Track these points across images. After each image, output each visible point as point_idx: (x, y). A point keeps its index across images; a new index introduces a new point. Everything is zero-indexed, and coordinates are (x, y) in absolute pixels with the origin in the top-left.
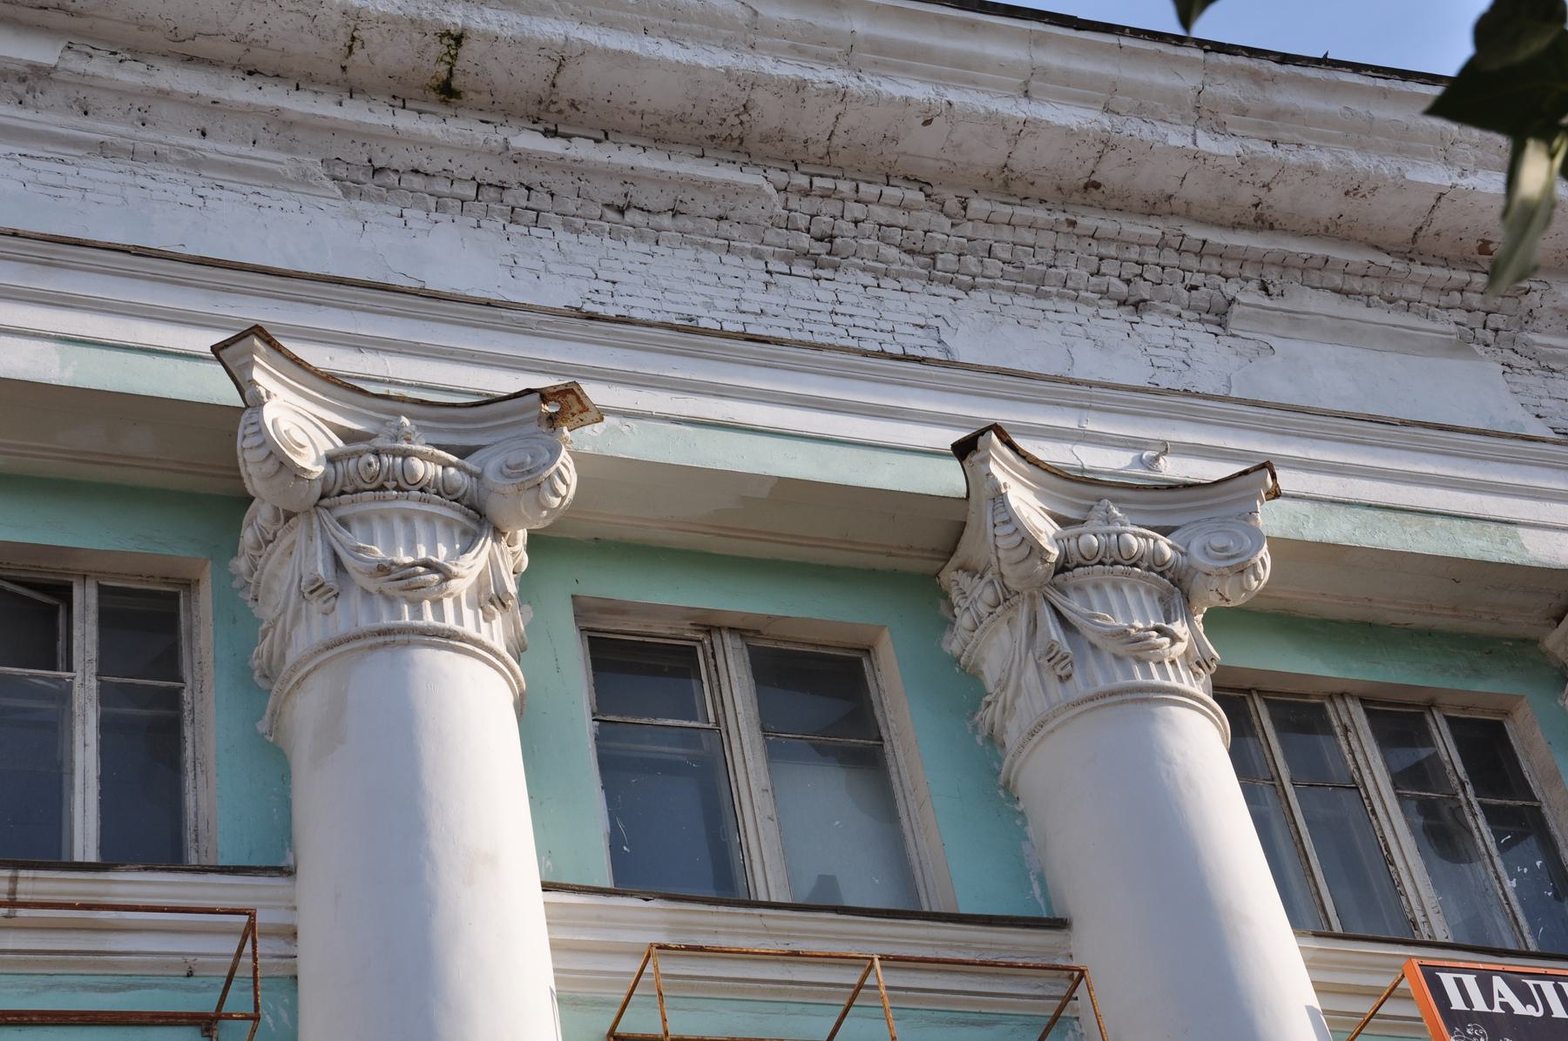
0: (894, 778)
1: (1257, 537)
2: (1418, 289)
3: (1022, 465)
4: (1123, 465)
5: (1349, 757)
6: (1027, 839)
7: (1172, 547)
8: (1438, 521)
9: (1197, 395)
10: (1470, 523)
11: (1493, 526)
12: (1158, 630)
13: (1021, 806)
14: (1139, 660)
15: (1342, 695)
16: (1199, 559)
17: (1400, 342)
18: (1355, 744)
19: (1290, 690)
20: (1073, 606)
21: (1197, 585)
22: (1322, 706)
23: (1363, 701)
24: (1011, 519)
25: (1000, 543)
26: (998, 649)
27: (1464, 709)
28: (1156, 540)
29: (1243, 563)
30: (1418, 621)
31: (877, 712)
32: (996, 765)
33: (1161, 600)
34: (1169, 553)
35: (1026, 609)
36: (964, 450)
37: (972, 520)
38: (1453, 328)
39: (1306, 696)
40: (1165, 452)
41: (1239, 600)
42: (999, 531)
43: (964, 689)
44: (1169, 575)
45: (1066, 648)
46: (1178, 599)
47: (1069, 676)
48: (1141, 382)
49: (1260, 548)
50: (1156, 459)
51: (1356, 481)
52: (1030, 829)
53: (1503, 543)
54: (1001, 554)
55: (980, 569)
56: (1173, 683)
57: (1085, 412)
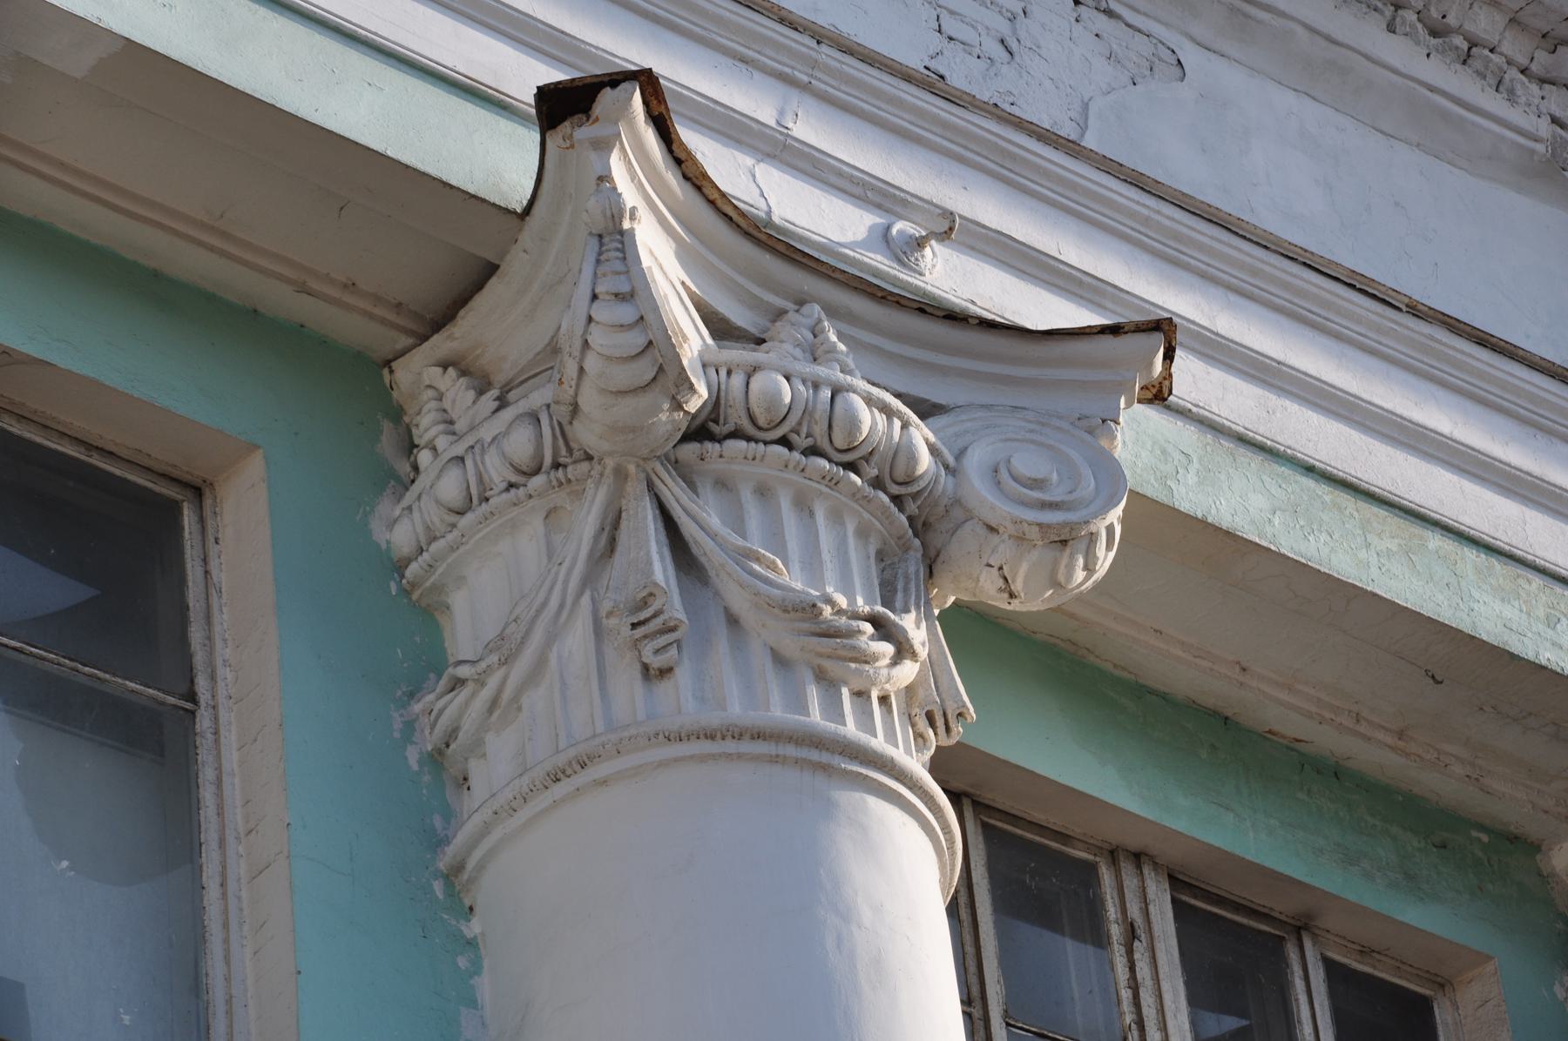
0: (207, 794)
1: (1110, 474)
2: (1500, 20)
3: (672, 178)
4: (848, 237)
5: (1126, 994)
6: (473, 1003)
7: (933, 450)
8: (1435, 541)
9: (1020, 124)
10: (1496, 564)
11: (1538, 581)
12: (875, 621)
13: (474, 928)
14: (821, 677)
15: (1138, 857)
16: (978, 489)
17: (1431, 126)
18: (1143, 971)
19: (1038, 816)
20: (704, 517)
21: (963, 546)
22: (1092, 868)
23: (1175, 882)
24: (633, 290)
25: (597, 338)
26: (503, 574)
27: (1365, 952)
28: (905, 426)
29: (1072, 527)
30: (1327, 740)
31: (196, 635)
32: (438, 822)
33: (881, 556)
34: (925, 461)
35: (601, 495)
36: (562, 106)
37: (515, 265)
38: (1544, 128)
39: (1065, 838)
40: (945, 236)
41: (1031, 601)
42: (602, 312)
43: (396, 637)
44: (912, 508)
45: (676, 610)
46: (914, 564)
47: (665, 672)
48: (914, 60)
49: (1112, 503)
50: (920, 243)
51: (1293, 408)
52: (485, 986)
53: (1552, 622)
54: (591, 363)
55: (499, 379)
56: (879, 743)
57: (795, 95)
